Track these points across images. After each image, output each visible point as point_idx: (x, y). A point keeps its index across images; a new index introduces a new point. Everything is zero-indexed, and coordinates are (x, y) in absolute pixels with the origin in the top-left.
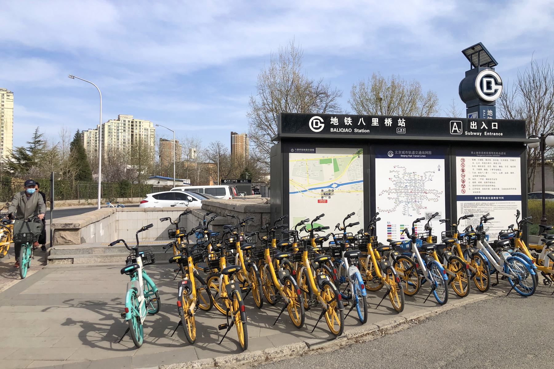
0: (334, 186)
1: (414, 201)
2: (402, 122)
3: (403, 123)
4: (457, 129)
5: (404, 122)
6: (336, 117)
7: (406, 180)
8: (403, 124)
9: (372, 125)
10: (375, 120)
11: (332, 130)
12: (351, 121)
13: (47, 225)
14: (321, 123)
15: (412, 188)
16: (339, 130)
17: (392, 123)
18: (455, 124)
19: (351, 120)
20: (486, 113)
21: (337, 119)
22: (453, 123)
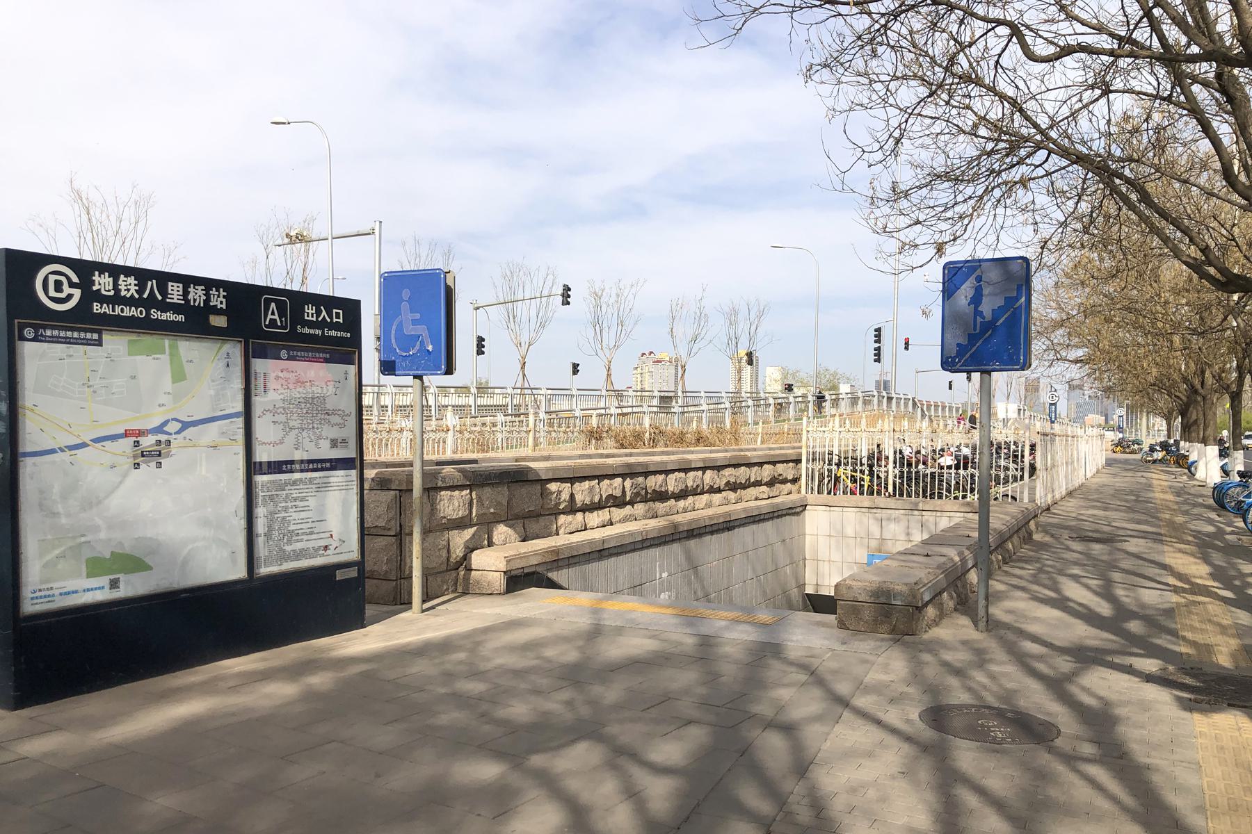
0: (173, 427)
1: (311, 426)
2: (219, 296)
3: (221, 299)
4: (276, 317)
5: (224, 297)
6: (107, 274)
7: (299, 392)
8: (221, 303)
9: (168, 300)
10: (175, 289)
11: (96, 308)
12: (137, 288)
14: (72, 285)
15: (308, 405)
16: (113, 311)
17: (205, 298)
18: (273, 305)
22: (268, 302)
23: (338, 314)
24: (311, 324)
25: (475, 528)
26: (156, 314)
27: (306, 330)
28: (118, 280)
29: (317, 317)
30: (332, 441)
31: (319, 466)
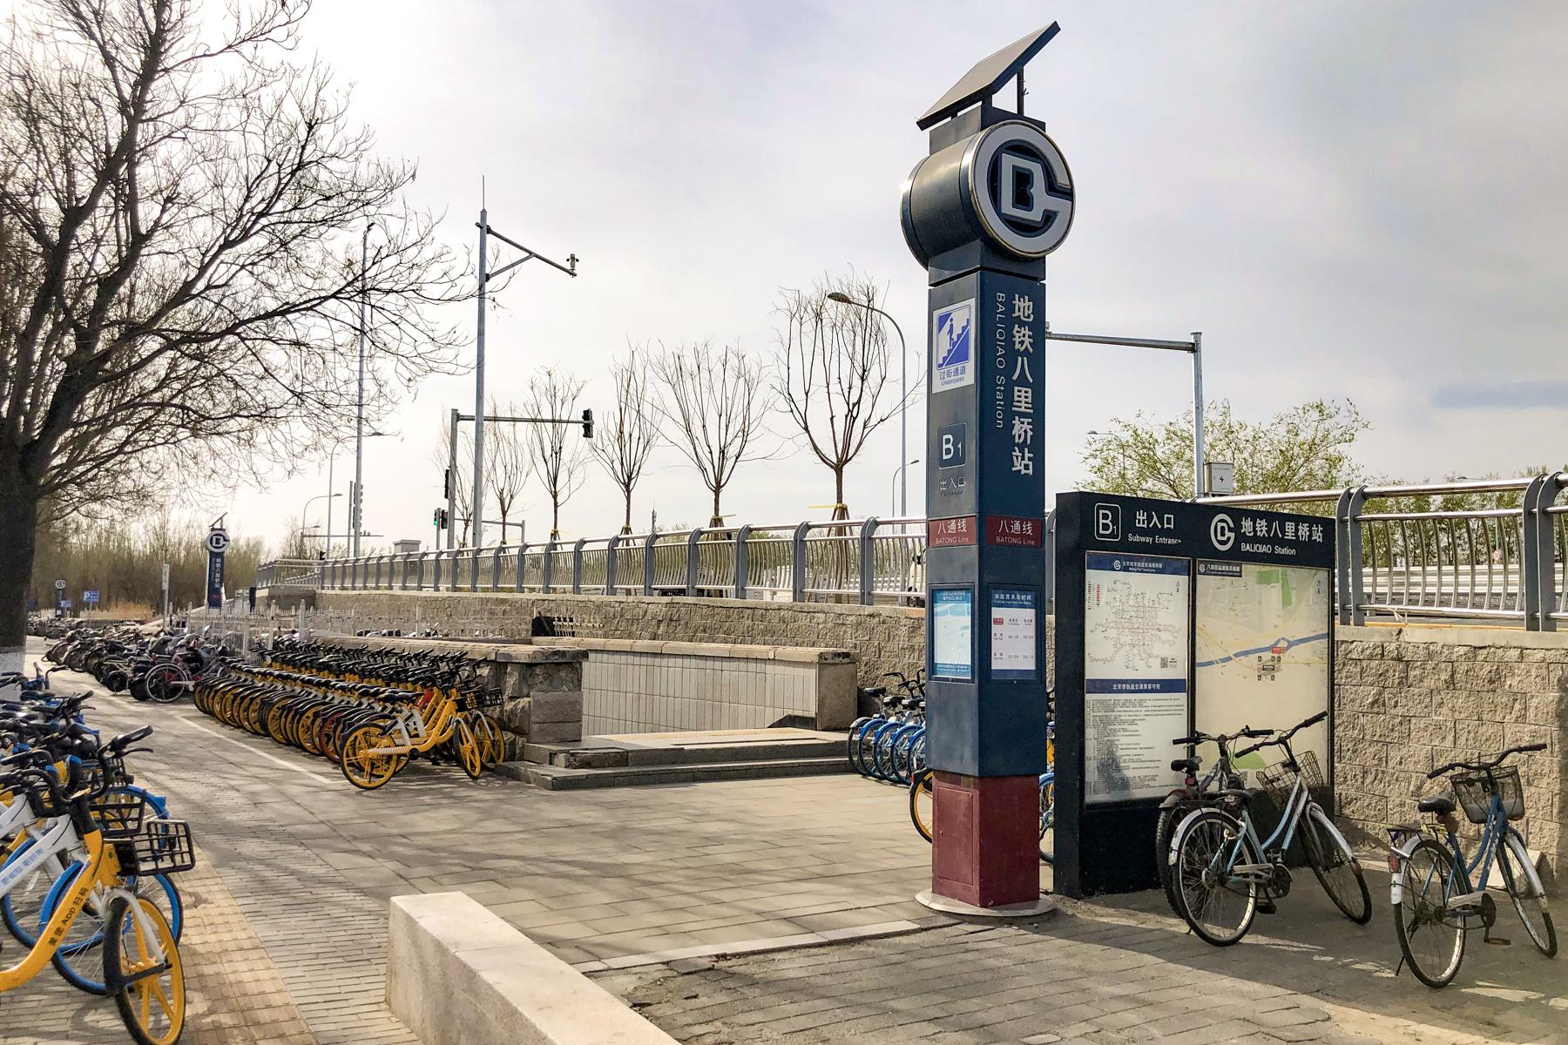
2: (1023, 459)
3: (1026, 462)
5: (1029, 459)
8: (1026, 467)
10: (1023, 394)
11: (1246, 547)
14: (1230, 530)
20: (1011, 308)
23: (1169, 519)
24: (1142, 532)
26: (1278, 550)
27: (1137, 539)
29: (1148, 524)
30: (1163, 659)
31: (1141, 687)
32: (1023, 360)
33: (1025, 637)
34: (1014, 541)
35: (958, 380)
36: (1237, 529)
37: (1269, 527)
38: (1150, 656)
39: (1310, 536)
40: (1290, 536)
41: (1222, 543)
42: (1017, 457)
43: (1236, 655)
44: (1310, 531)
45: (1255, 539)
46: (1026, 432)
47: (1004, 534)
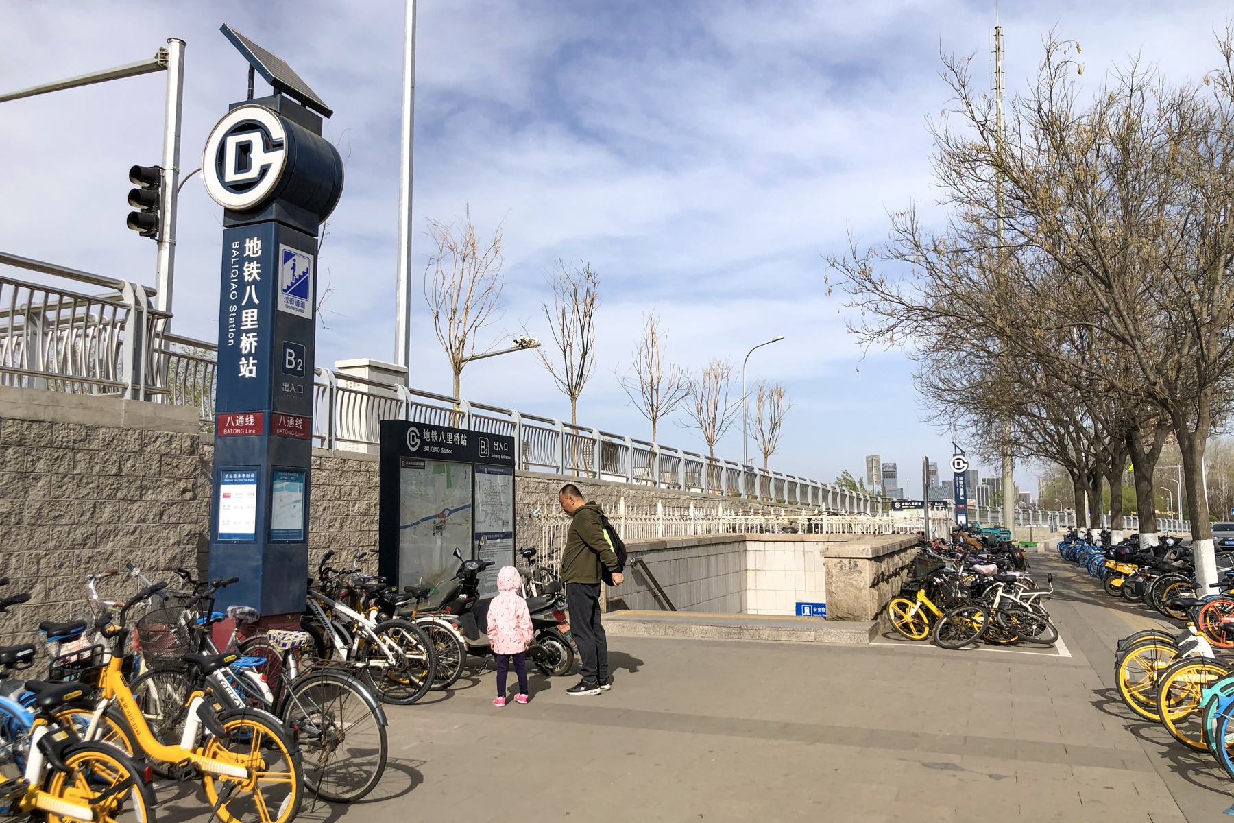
0: (447, 513)
2: (248, 366)
3: (251, 367)
5: (254, 365)
8: (251, 371)
9: (242, 328)
10: (250, 315)
11: (426, 449)
12: (256, 339)
13: (405, 527)
17: (256, 344)
19: (257, 268)
20: (242, 249)
21: (259, 242)
25: (282, 660)
28: (244, 265)
32: (251, 288)
33: (248, 507)
34: (238, 431)
35: (299, 310)
36: (421, 437)
37: (439, 435)
38: (499, 519)
39: (460, 441)
40: (449, 442)
41: (413, 446)
42: (243, 365)
43: (422, 520)
44: (460, 438)
45: (431, 444)
46: (251, 344)
47: (230, 427)
